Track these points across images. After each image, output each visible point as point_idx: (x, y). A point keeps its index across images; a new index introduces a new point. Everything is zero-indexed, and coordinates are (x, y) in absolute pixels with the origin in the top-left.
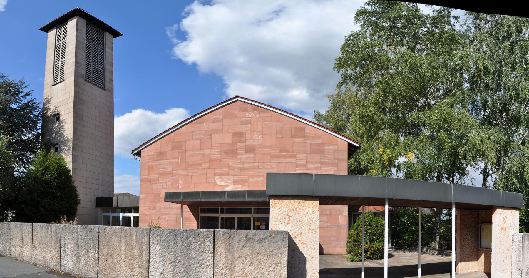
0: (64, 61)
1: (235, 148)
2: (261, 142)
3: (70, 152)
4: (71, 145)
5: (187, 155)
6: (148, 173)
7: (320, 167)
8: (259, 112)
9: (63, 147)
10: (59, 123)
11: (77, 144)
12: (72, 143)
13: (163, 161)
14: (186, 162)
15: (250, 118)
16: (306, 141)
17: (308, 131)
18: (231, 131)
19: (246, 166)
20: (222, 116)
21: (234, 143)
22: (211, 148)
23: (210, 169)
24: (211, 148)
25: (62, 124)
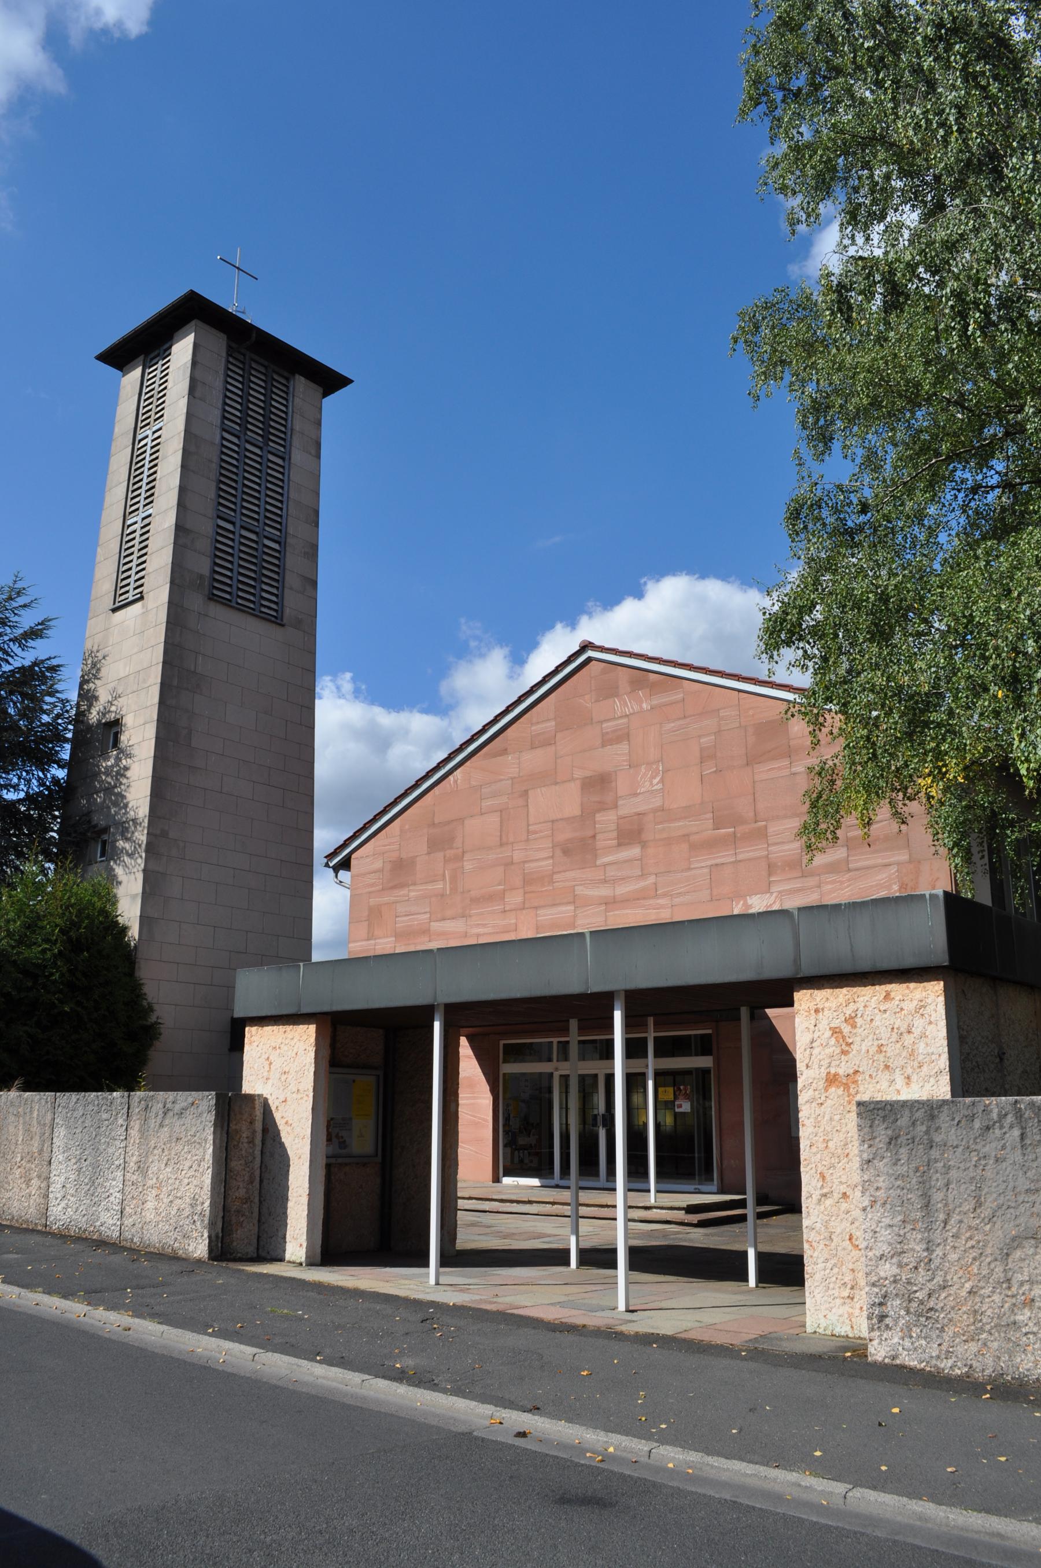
0: (150, 515)
1: (590, 833)
2: (657, 802)
3: (139, 861)
4: (141, 836)
5: (468, 866)
6: (368, 933)
7: (847, 861)
8: (648, 690)
9: (121, 844)
10: (118, 754)
11: (164, 834)
12: (146, 832)
13: (404, 892)
14: (463, 892)
15: (625, 720)
16: (793, 770)
17: (796, 728)
18: (578, 774)
19: (621, 890)
20: (553, 723)
21: (587, 815)
22: (528, 840)
23: (524, 912)
24: (528, 840)
25: (124, 762)
